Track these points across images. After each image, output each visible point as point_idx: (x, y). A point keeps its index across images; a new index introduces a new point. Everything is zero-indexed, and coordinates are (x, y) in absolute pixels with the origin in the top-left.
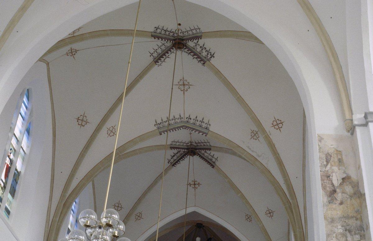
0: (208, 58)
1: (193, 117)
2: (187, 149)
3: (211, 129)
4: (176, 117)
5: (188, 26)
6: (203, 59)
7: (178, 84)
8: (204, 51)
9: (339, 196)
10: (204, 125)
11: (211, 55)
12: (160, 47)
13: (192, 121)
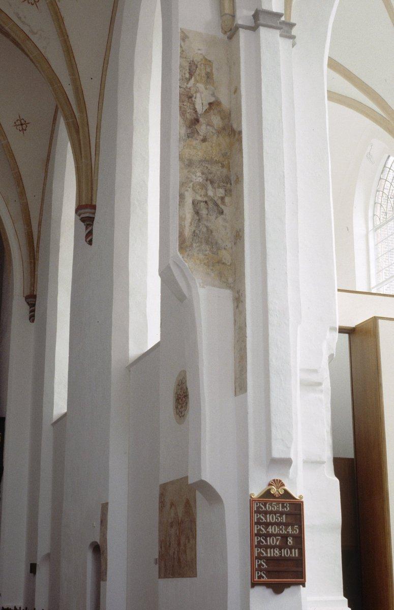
9: (203, 129)
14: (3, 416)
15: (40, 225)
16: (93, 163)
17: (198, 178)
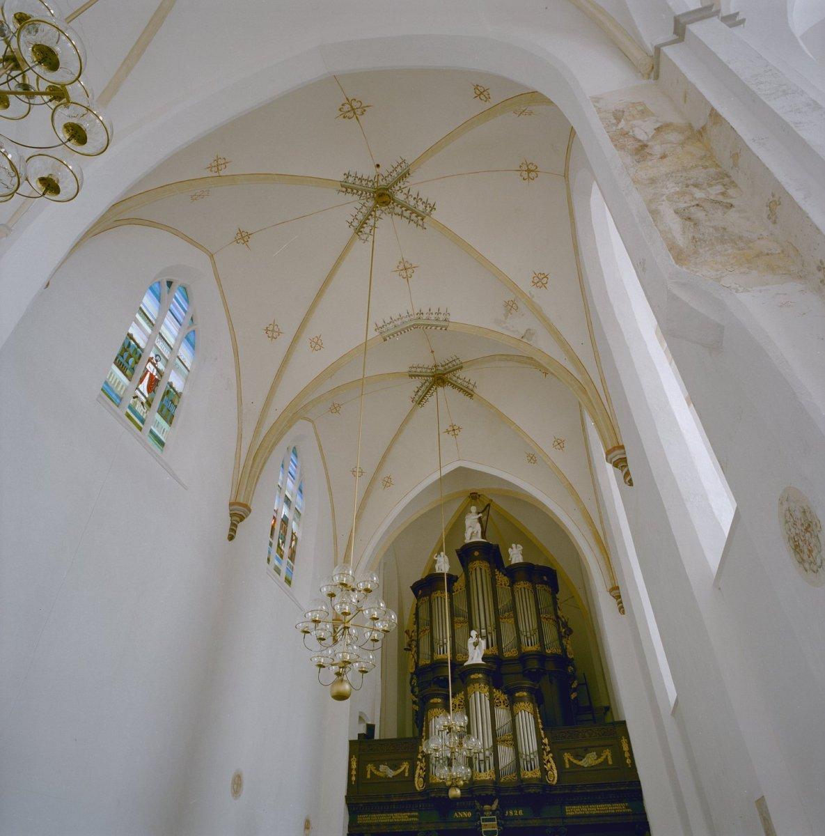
0: (427, 212)
1: (425, 310)
2: (433, 376)
3: (452, 319)
4: (402, 315)
5: (443, 356)
6: (418, 215)
7: (396, 269)
8: (420, 203)
10: (442, 317)
11: (430, 207)
12: (359, 211)
13: (425, 317)
14: (605, 704)
15: (602, 522)
16: (607, 407)
17: (672, 188)
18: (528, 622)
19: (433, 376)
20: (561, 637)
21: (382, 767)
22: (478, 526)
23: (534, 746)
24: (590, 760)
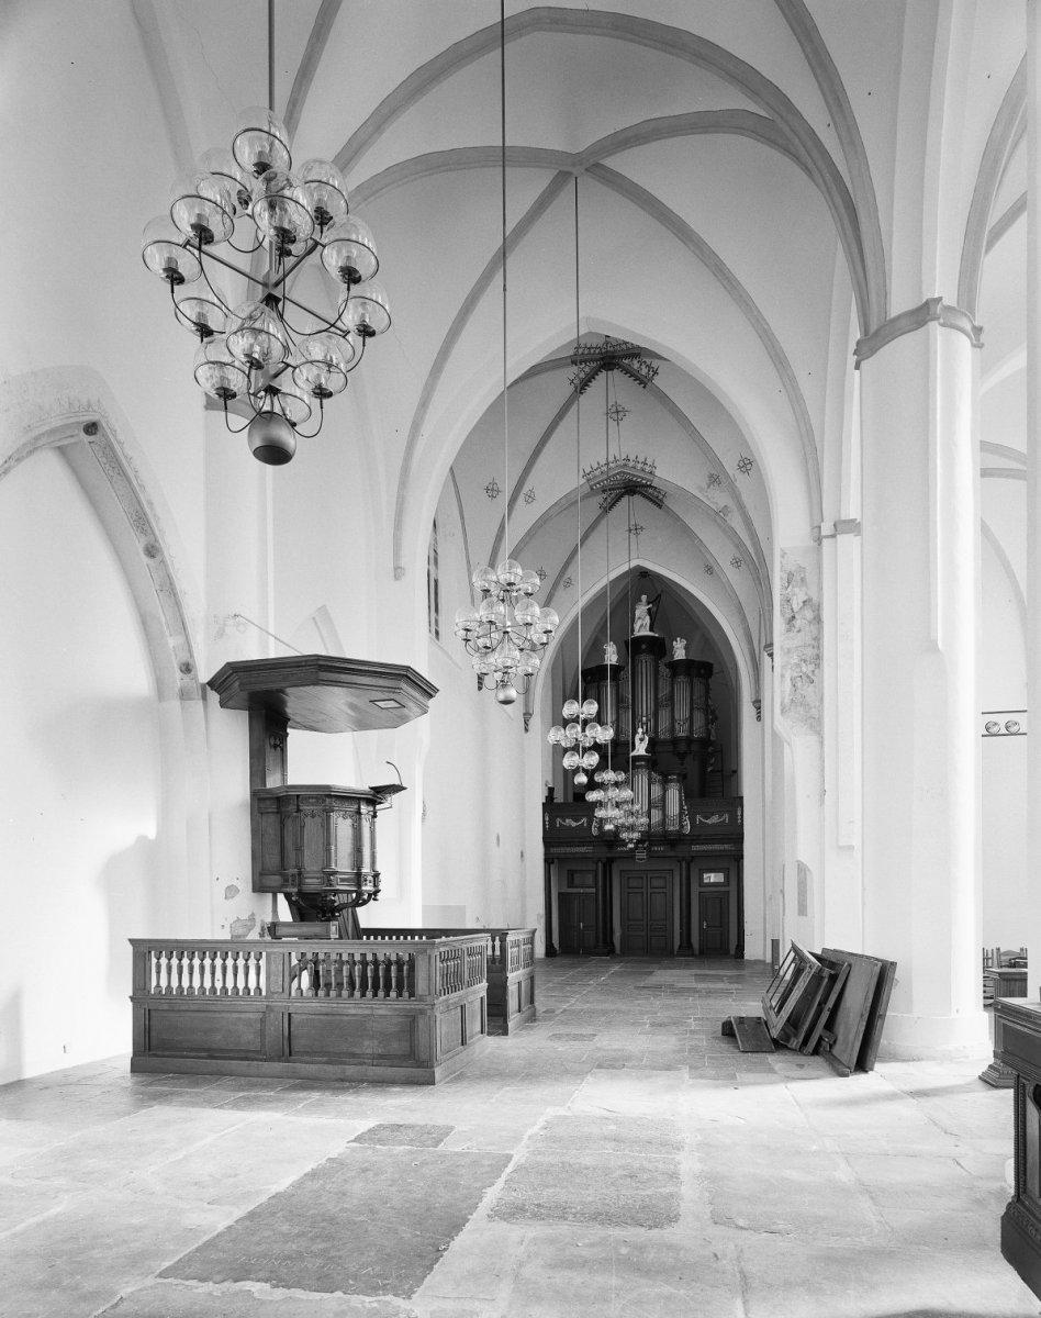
1: (632, 457)
8: (643, 367)
9: (798, 623)
10: (648, 469)
13: (631, 464)
17: (795, 659)
18: (682, 712)
19: (602, 359)
20: (707, 723)
21: (567, 821)
22: (648, 617)
23: (677, 811)
24: (714, 820)
